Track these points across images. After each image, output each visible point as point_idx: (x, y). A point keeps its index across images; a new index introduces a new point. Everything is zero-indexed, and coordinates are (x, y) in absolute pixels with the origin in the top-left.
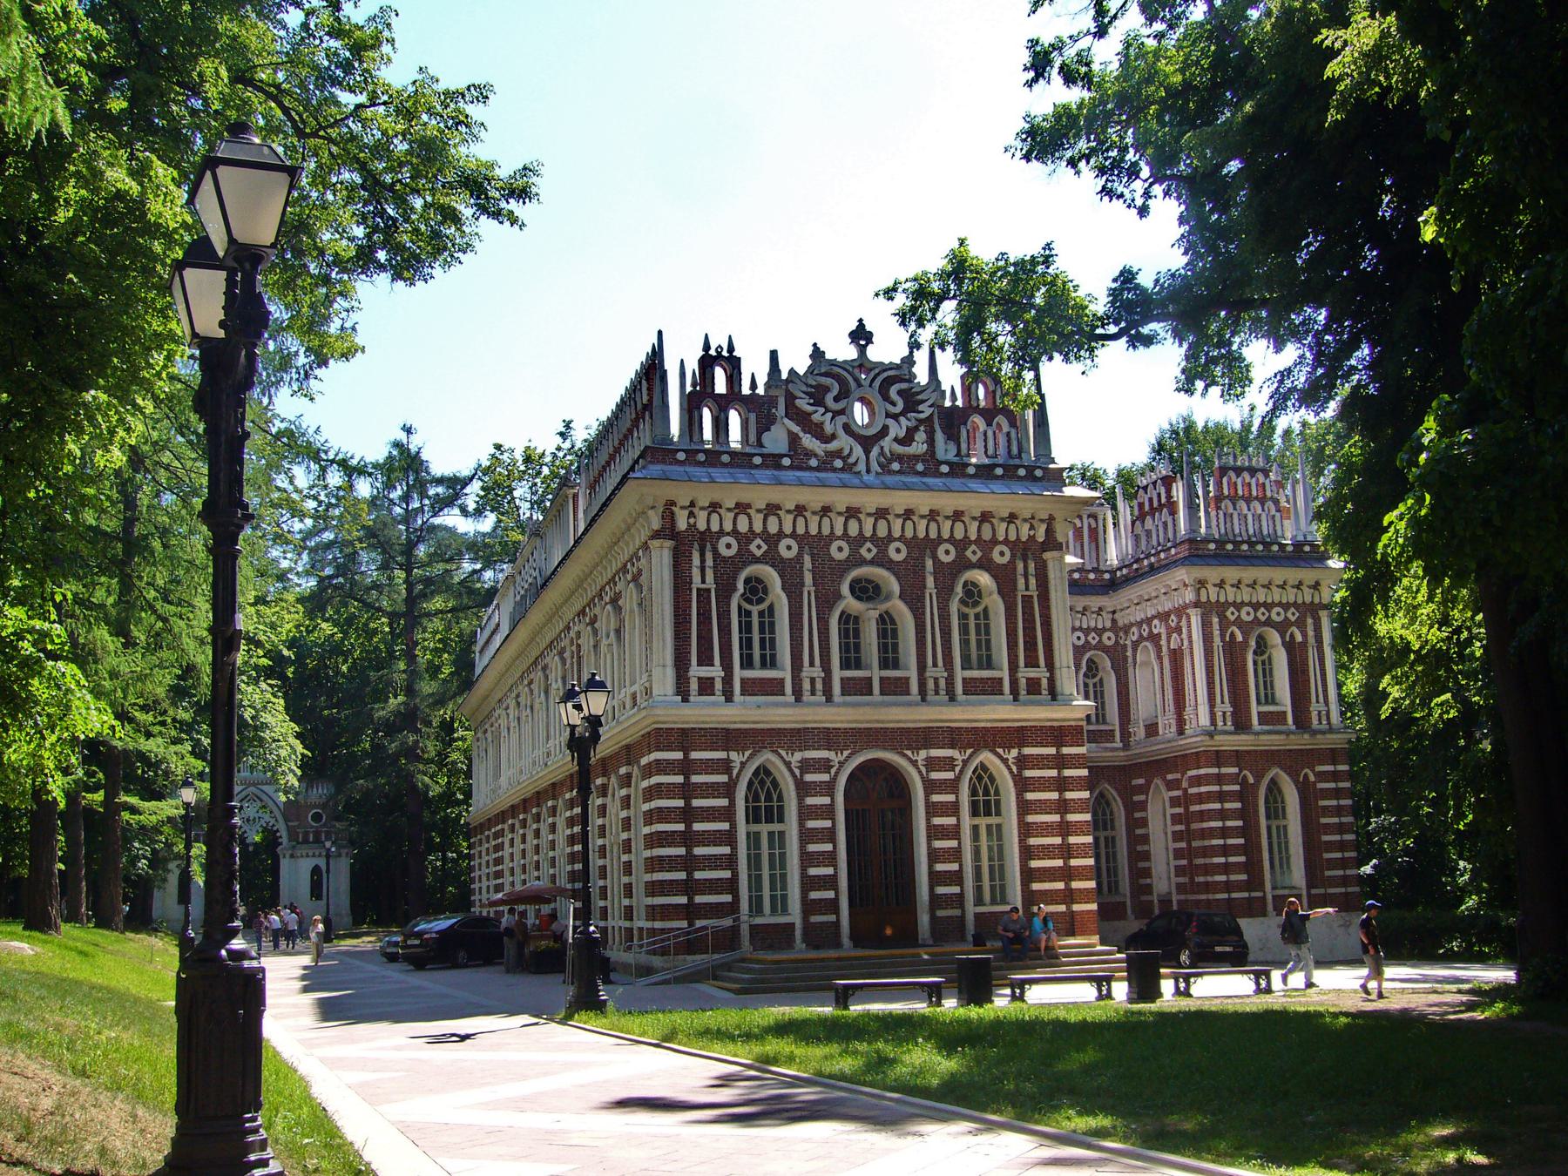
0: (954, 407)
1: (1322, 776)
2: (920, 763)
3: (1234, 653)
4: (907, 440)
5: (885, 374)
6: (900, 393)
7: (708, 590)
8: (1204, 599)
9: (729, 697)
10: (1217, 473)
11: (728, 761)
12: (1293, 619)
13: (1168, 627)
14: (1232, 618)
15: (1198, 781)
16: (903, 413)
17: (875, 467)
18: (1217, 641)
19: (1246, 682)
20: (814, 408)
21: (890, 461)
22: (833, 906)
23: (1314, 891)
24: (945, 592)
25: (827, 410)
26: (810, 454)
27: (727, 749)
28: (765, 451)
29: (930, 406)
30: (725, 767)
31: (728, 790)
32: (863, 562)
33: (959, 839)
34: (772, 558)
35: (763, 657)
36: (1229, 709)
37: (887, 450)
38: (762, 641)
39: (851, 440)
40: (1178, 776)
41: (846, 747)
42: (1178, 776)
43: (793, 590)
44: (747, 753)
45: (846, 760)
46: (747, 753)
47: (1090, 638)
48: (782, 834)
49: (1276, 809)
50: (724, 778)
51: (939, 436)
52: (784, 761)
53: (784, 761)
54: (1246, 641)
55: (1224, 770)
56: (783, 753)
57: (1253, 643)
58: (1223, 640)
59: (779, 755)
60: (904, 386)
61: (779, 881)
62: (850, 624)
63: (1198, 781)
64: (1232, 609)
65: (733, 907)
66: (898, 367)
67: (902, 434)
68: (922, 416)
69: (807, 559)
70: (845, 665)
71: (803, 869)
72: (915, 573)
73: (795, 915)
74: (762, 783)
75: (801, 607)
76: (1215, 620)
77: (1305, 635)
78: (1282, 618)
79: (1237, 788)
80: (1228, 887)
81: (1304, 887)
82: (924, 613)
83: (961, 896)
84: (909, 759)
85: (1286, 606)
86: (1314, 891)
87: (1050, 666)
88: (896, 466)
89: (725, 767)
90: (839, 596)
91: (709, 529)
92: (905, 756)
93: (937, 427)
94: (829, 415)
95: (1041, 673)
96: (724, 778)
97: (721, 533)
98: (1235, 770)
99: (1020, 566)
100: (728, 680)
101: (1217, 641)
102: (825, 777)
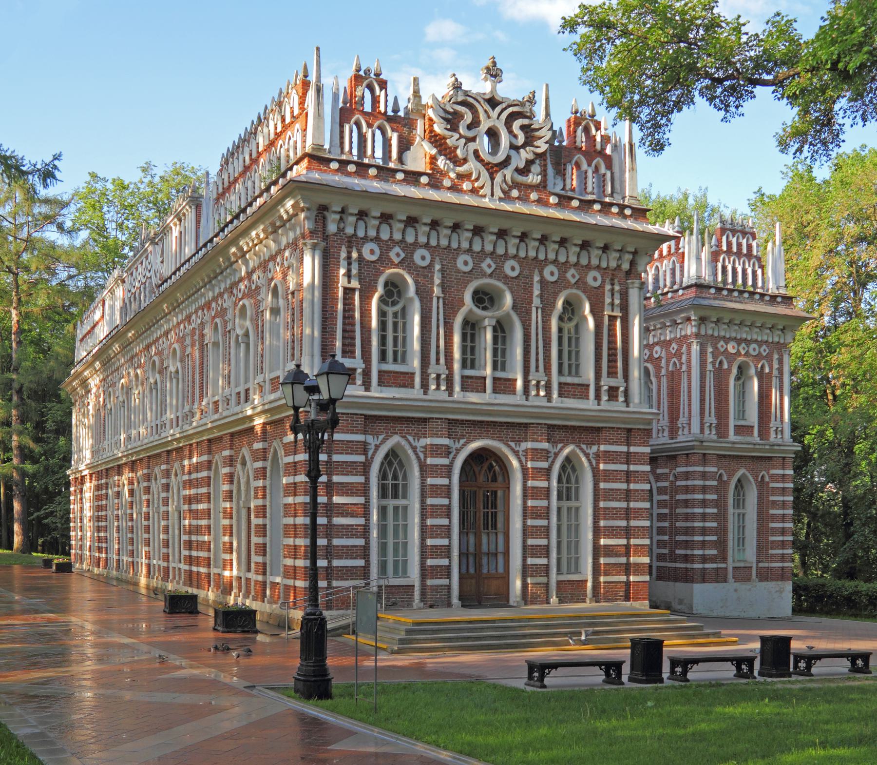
0: (560, 147)
1: (773, 478)
2: (521, 453)
3: (721, 375)
4: (524, 171)
5: (510, 110)
6: (523, 128)
7: (353, 290)
8: (703, 332)
9: (367, 385)
10: (719, 233)
11: (365, 444)
12: (764, 354)
13: (668, 352)
14: (722, 350)
15: (687, 476)
16: (524, 146)
17: (498, 193)
18: (710, 367)
19: (727, 401)
20: (450, 133)
21: (511, 188)
22: (446, 572)
23: (761, 565)
24: (547, 308)
25: (461, 137)
26: (444, 174)
27: (365, 433)
28: (406, 168)
29: (546, 143)
30: (363, 448)
31: (365, 469)
32: (484, 275)
33: (548, 519)
34: (407, 263)
35: (395, 353)
36: (715, 422)
37: (508, 178)
38: (395, 339)
39: (479, 165)
40: (667, 471)
41: (463, 436)
42: (667, 471)
43: (424, 294)
44: (381, 437)
45: (462, 448)
46: (381, 437)
47: (762, 350)
48: (405, 508)
49: (568, 489)
50: (361, 458)
51: (550, 171)
52: (411, 445)
53: (411, 445)
54: (729, 370)
55: (708, 469)
56: (411, 438)
57: (735, 371)
58: (714, 367)
59: (407, 440)
60: (526, 122)
61: (402, 548)
62: (471, 328)
63: (687, 476)
64: (722, 343)
65: (365, 572)
66: (522, 104)
67: (522, 165)
68: (539, 151)
69: (438, 267)
70: (464, 365)
71: (423, 540)
72: (525, 289)
73: (414, 575)
74: (390, 464)
75: (431, 310)
76: (710, 350)
77: (771, 368)
78: (756, 353)
79: (715, 483)
80: (704, 559)
81: (754, 559)
82: (530, 325)
83: (547, 567)
84: (512, 449)
85: (760, 343)
86: (761, 565)
87: (626, 377)
88: (515, 193)
89: (363, 448)
90: (462, 303)
91: (355, 235)
92: (509, 446)
93: (548, 161)
94: (463, 141)
95: (618, 382)
96: (361, 458)
97: (366, 239)
98: (715, 469)
99: (608, 287)
100: (367, 373)
101: (710, 367)
102: (445, 461)
